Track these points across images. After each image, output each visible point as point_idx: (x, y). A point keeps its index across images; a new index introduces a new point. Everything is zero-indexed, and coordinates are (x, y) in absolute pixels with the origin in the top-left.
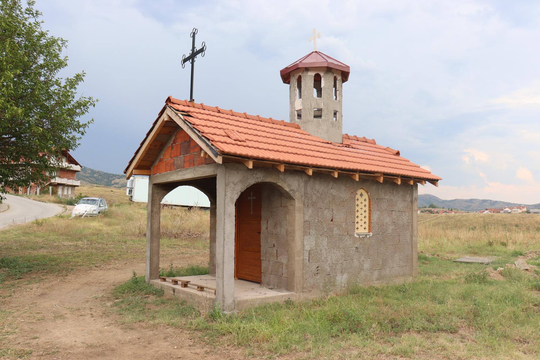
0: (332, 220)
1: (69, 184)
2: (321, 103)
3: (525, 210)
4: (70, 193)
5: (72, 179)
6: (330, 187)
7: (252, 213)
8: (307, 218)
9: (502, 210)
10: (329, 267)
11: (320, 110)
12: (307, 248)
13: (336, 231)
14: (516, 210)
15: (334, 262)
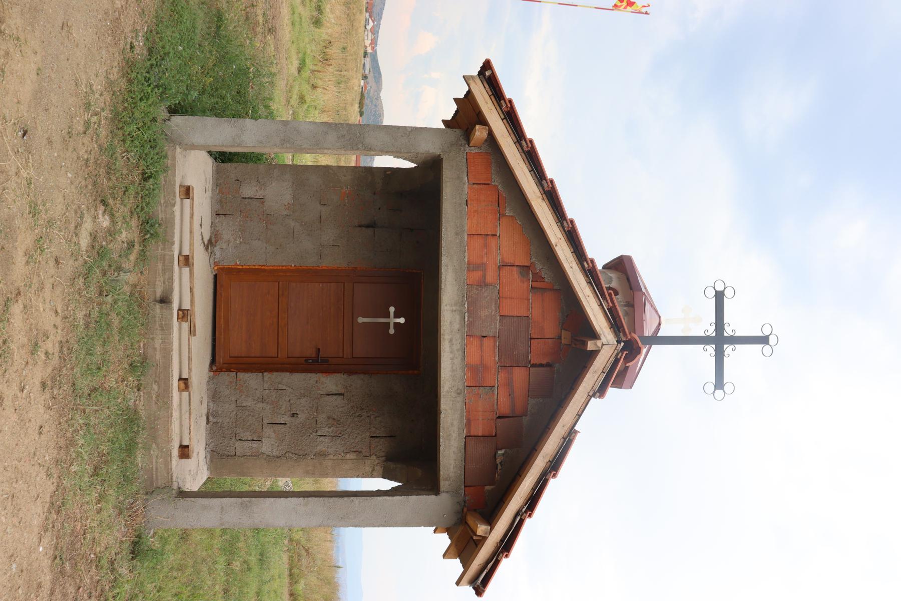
3: (369, 50)
7: (361, 320)
9: (371, 16)
14: (370, 38)
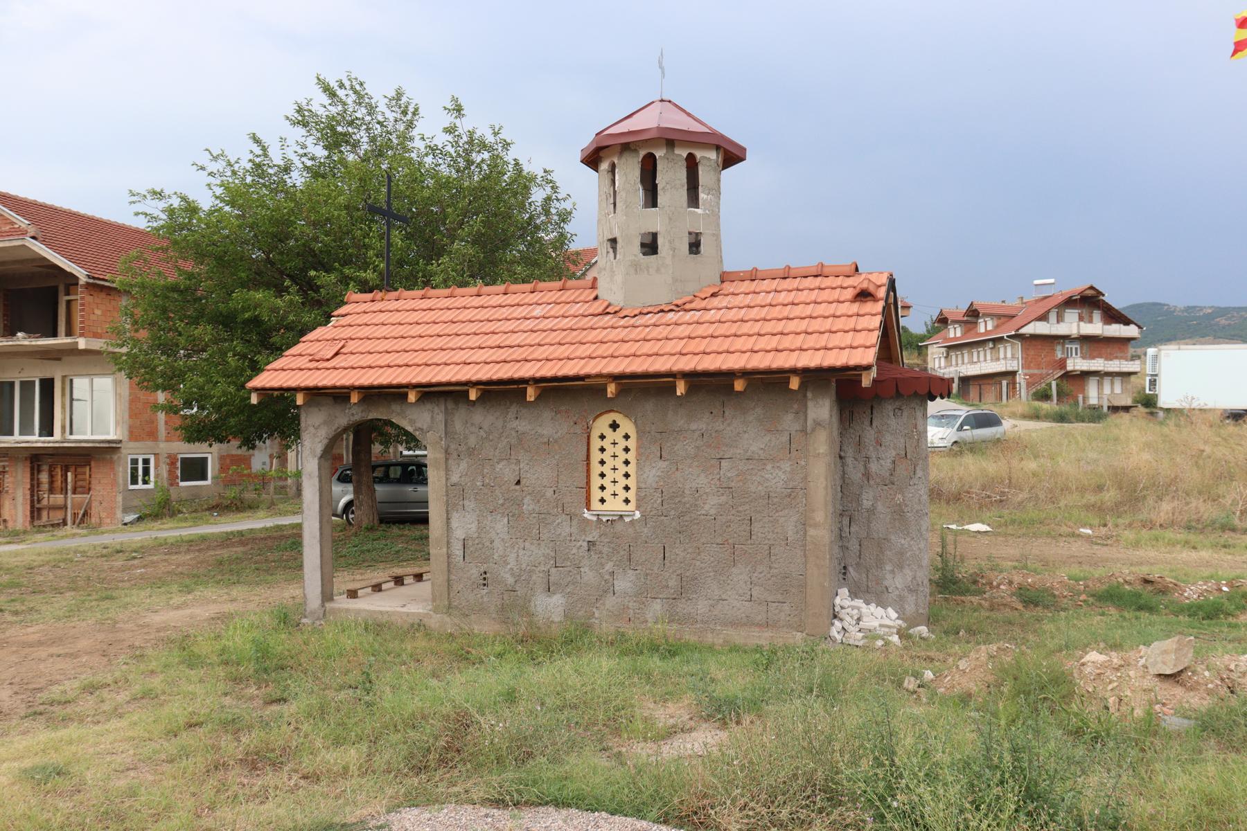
0: (518, 483)
1: (1111, 369)
2: (654, 221)
4: (1118, 390)
5: (1121, 358)
6: (511, 415)
8: (455, 478)
10: (512, 575)
11: (654, 236)
12: (459, 534)
13: (528, 505)
15: (524, 566)
